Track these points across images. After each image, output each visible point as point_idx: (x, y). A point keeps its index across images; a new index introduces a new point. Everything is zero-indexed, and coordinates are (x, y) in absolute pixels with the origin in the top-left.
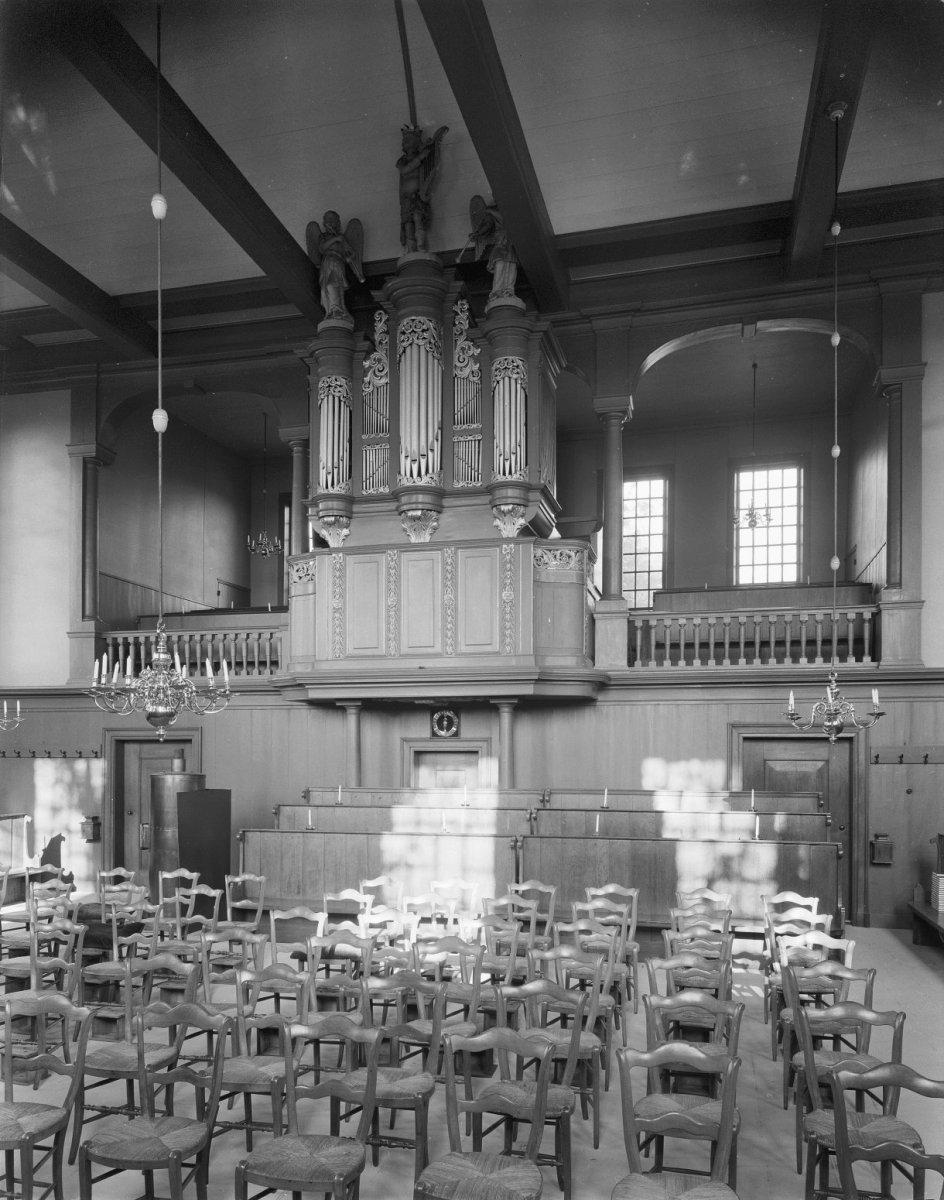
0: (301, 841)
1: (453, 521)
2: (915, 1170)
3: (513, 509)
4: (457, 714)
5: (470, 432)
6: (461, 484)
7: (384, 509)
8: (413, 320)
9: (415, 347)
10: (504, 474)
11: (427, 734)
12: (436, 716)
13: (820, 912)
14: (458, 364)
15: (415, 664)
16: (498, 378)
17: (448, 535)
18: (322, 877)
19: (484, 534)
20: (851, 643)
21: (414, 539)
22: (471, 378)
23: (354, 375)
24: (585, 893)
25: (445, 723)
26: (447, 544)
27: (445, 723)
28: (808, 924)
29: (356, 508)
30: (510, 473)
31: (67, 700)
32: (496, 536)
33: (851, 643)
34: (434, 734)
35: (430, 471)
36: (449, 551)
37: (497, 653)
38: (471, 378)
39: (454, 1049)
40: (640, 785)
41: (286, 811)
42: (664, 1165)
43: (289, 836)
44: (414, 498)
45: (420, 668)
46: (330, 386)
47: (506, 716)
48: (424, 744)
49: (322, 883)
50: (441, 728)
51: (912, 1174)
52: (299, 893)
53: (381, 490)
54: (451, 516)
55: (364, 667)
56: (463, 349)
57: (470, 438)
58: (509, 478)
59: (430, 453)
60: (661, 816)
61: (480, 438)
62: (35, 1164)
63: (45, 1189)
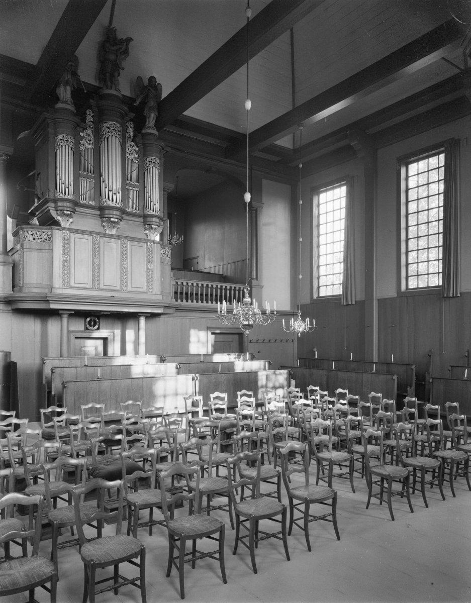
0: (98, 385)
1: (127, 227)
2: (23, 541)
3: (70, 214)
4: (99, 319)
5: (134, 186)
6: (130, 210)
7: (91, 212)
8: (115, 124)
9: (114, 137)
10: (65, 194)
11: (82, 328)
12: (88, 319)
13: (301, 392)
14: (128, 151)
15: (109, 294)
16: (62, 144)
17: (124, 233)
18: (109, 402)
19: (143, 237)
20: (199, 295)
21: (107, 232)
22: (134, 160)
23: (78, 140)
24: (81, 408)
25: (92, 323)
26: (125, 237)
27: (92, 323)
28: (297, 397)
29: (77, 209)
30: (69, 194)
31: (184, 313)
32: (146, 238)
33: (199, 295)
34: (87, 329)
35: (118, 201)
36: (125, 241)
37: (146, 293)
38: (134, 160)
39: (454, 420)
40: (188, 351)
41: (57, 371)
42: (276, 485)
43: (91, 383)
44: (111, 212)
45: (112, 296)
46: (67, 140)
47: (65, 320)
48: (81, 333)
49: (109, 405)
50: (91, 326)
51: (21, 543)
52: (97, 412)
53: (91, 202)
54: (125, 224)
55: (80, 293)
56: (131, 145)
57: (134, 189)
58: (154, 213)
59: (118, 194)
60: (130, 369)
61: (138, 190)
62: (212, 536)
63: (242, 539)
